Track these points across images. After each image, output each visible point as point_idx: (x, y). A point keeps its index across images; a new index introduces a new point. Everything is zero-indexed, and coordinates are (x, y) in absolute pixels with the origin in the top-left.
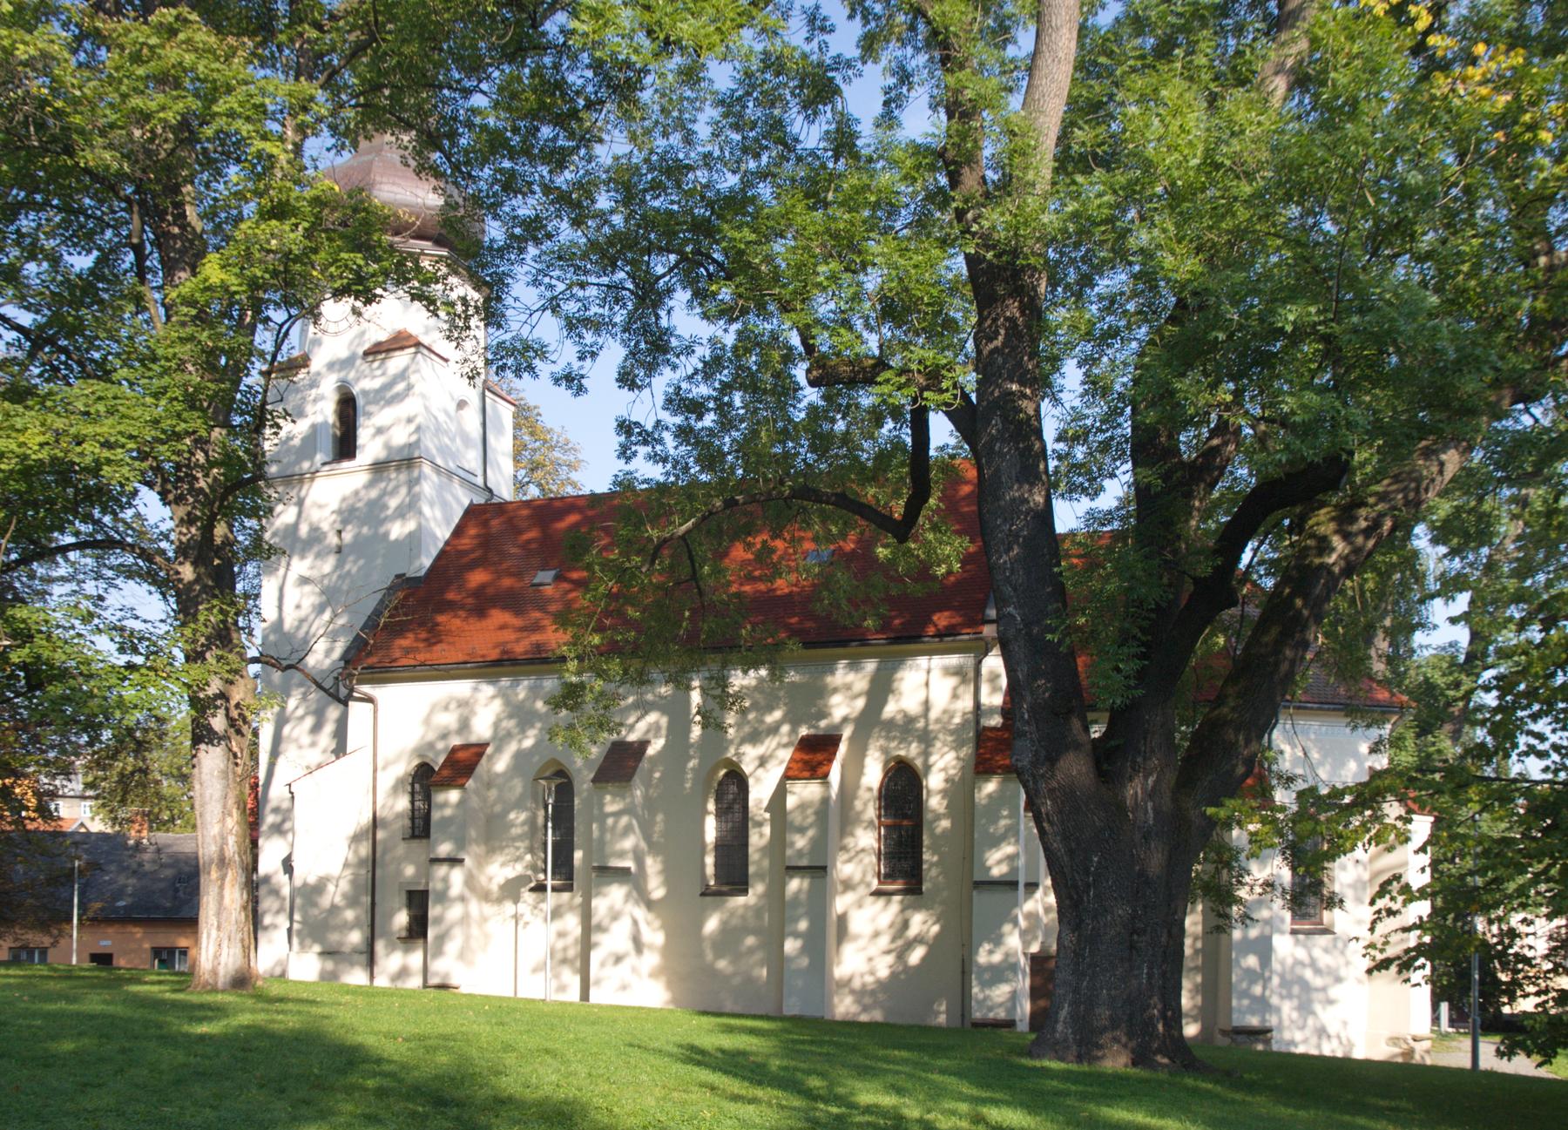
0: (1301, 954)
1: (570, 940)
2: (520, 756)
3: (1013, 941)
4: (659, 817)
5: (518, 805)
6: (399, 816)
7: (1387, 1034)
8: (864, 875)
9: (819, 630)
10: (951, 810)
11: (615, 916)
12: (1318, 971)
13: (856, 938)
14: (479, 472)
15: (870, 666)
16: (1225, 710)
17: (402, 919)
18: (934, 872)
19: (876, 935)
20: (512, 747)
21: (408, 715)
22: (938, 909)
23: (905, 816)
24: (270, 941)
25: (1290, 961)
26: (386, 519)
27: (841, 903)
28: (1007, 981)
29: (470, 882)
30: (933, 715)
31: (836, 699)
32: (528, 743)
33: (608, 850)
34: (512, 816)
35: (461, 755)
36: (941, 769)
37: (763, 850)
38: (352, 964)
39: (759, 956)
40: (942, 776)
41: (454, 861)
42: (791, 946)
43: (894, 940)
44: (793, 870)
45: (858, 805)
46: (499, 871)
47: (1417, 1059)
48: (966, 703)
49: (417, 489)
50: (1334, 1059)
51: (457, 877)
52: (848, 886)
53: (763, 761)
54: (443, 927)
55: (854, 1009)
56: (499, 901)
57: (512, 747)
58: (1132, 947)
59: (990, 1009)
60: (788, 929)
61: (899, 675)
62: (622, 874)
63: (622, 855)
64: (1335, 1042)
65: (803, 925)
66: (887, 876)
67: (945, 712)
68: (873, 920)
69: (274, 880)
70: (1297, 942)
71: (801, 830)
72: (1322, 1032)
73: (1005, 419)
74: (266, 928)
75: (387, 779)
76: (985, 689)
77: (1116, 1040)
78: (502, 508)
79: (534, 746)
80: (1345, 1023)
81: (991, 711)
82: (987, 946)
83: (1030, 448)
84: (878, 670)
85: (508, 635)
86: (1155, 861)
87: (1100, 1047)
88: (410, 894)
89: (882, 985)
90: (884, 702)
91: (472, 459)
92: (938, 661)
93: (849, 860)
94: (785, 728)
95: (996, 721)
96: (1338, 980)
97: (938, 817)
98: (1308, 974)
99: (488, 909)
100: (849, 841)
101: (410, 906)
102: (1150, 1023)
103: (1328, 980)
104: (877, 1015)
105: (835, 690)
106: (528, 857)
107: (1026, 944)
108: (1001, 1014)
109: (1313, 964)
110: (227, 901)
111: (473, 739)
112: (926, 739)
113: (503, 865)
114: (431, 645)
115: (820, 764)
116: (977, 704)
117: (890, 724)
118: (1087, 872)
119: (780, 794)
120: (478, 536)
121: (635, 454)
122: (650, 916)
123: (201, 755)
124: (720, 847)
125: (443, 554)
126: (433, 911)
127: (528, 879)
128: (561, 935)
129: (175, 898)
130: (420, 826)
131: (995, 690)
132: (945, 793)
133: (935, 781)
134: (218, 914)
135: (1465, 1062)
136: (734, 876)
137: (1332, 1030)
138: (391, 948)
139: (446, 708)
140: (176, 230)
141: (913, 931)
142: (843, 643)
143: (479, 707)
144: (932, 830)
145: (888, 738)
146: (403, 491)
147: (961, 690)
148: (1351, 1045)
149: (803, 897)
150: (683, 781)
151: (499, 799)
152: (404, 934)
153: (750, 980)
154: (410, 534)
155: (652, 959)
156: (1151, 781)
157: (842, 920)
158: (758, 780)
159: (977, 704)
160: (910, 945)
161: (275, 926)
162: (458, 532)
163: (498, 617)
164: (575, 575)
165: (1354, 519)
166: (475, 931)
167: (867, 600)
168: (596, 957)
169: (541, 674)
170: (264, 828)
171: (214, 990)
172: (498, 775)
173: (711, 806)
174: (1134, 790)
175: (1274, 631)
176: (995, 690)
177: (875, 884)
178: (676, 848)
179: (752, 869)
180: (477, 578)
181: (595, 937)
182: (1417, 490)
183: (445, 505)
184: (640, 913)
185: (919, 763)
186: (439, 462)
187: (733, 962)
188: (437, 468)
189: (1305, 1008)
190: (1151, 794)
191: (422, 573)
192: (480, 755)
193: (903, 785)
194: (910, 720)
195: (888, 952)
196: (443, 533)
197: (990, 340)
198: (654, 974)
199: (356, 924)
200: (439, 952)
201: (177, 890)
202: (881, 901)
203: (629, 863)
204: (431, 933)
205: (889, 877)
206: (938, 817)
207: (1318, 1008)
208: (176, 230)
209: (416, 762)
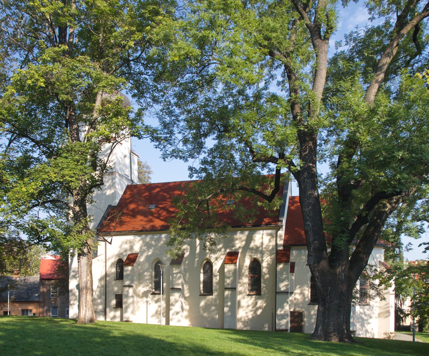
0: (362, 310)
1: (162, 308)
2: (147, 257)
3: (287, 308)
4: (187, 274)
5: (147, 270)
6: (112, 273)
7: (383, 332)
8: (245, 289)
9: (233, 222)
10: (269, 272)
11: (176, 301)
12: (366, 315)
13: (243, 307)
14: (130, 176)
15: (247, 233)
16: (360, 249)
17: (114, 302)
18: (264, 289)
19: (248, 306)
20: (145, 254)
21: (116, 245)
22: (265, 299)
23: (256, 274)
24: (73, 308)
25: (359, 313)
26: (105, 189)
27: (239, 297)
28: (285, 319)
29: (134, 292)
30: (264, 246)
31: (237, 242)
32: (150, 253)
33: (174, 283)
34: (145, 273)
35: (131, 256)
36: (266, 261)
37: (217, 283)
38: (100, 315)
39: (215, 312)
40: (266, 263)
41: (130, 286)
42: (226, 309)
43: (253, 307)
44: (227, 289)
45: (243, 271)
46: (142, 289)
47: (391, 338)
48: (273, 243)
49: (114, 181)
50: (370, 338)
51: (131, 290)
52: (240, 293)
53: (217, 259)
54: (127, 304)
55: (242, 326)
56: (142, 297)
57: (145, 254)
58: (339, 311)
59: (281, 326)
60: (225, 305)
61: (254, 236)
62: (179, 290)
63: (178, 284)
64: (370, 334)
65: (229, 304)
66: (251, 290)
67: (267, 245)
68: (247, 302)
69: (73, 291)
70: (361, 308)
71: (229, 278)
72: (367, 331)
73: (308, 173)
74: (71, 305)
75: (109, 263)
76: (278, 239)
77: (335, 335)
78: (136, 186)
79: (152, 254)
80: (372, 329)
81: (280, 245)
82: (280, 309)
83: (314, 181)
84: (249, 234)
85: (143, 223)
86: (344, 288)
87: (331, 337)
88: (116, 295)
89: (251, 320)
90: (250, 243)
91: (127, 172)
92: (265, 232)
93: (241, 286)
94: (223, 250)
95: (281, 248)
96: (371, 317)
97: (265, 274)
98: (363, 316)
99: (139, 300)
100: (241, 281)
101: (116, 298)
102: (343, 330)
103: (368, 318)
104: (248, 328)
105: (237, 239)
106: (150, 285)
107: (290, 308)
108: (284, 327)
109: (365, 313)
110: (88, 299)
111: (134, 252)
112: (262, 253)
113: (143, 287)
114: (121, 225)
115: (234, 260)
116: (276, 244)
117: (252, 249)
118: (327, 292)
119: (222, 268)
120: (130, 194)
121: (193, 176)
122: (185, 301)
123: (81, 259)
124: (204, 282)
125: (121, 199)
126: (124, 300)
127: (150, 291)
128: (160, 306)
129: (28, 295)
130: (120, 276)
131: (281, 240)
132: (267, 268)
133: (264, 264)
134: (86, 303)
135: (412, 340)
136: (208, 289)
137: (369, 331)
138: (111, 310)
139: (126, 243)
140: (73, 114)
141: (258, 305)
142: (239, 227)
143: (137, 243)
144: (264, 278)
145: (251, 253)
146: (110, 181)
147: (272, 239)
148: (374, 335)
149: (229, 296)
150: (194, 264)
151: (141, 269)
152: (115, 306)
153: (213, 319)
154: (113, 193)
155: (185, 313)
156: (343, 268)
157: (239, 302)
158: (215, 264)
159: (276, 244)
160: (257, 309)
161: (74, 304)
162: (125, 193)
163: (140, 217)
164: (161, 206)
165: (392, 199)
166: (136, 305)
167: (250, 216)
168: (171, 313)
169: (154, 234)
170: (70, 276)
171: (85, 323)
172: (141, 262)
173: (202, 271)
174: (339, 270)
175: (372, 228)
176: (281, 240)
177: (248, 293)
178: (192, 282)
179: (214, 288)
180: (132, 206)
181: (171, 307)
182: (408, 192)
183: (121, 185)
184: (183, 300)
185: (260, 259)
186: (120, 173)
187: (209, 314)
188: (120, 175)
189: (363, 325)
190: (343, 271)
191: (116, 205)
192: (137, 257)
193: (256, 266)
194: (257, 248)
195: (252, 311)
196: (121, 193)
197: (305, 152)
198: (186, 317)
199: (101, 303)
200: (126, 311)
201: (28, 293)
202: (250, 297)
203: (180, 287)
204: (124, 306)
205: (251, 290)
206: (265, 274)
207: (366, 325)
208: (73, 114)
209: (118, 258)
